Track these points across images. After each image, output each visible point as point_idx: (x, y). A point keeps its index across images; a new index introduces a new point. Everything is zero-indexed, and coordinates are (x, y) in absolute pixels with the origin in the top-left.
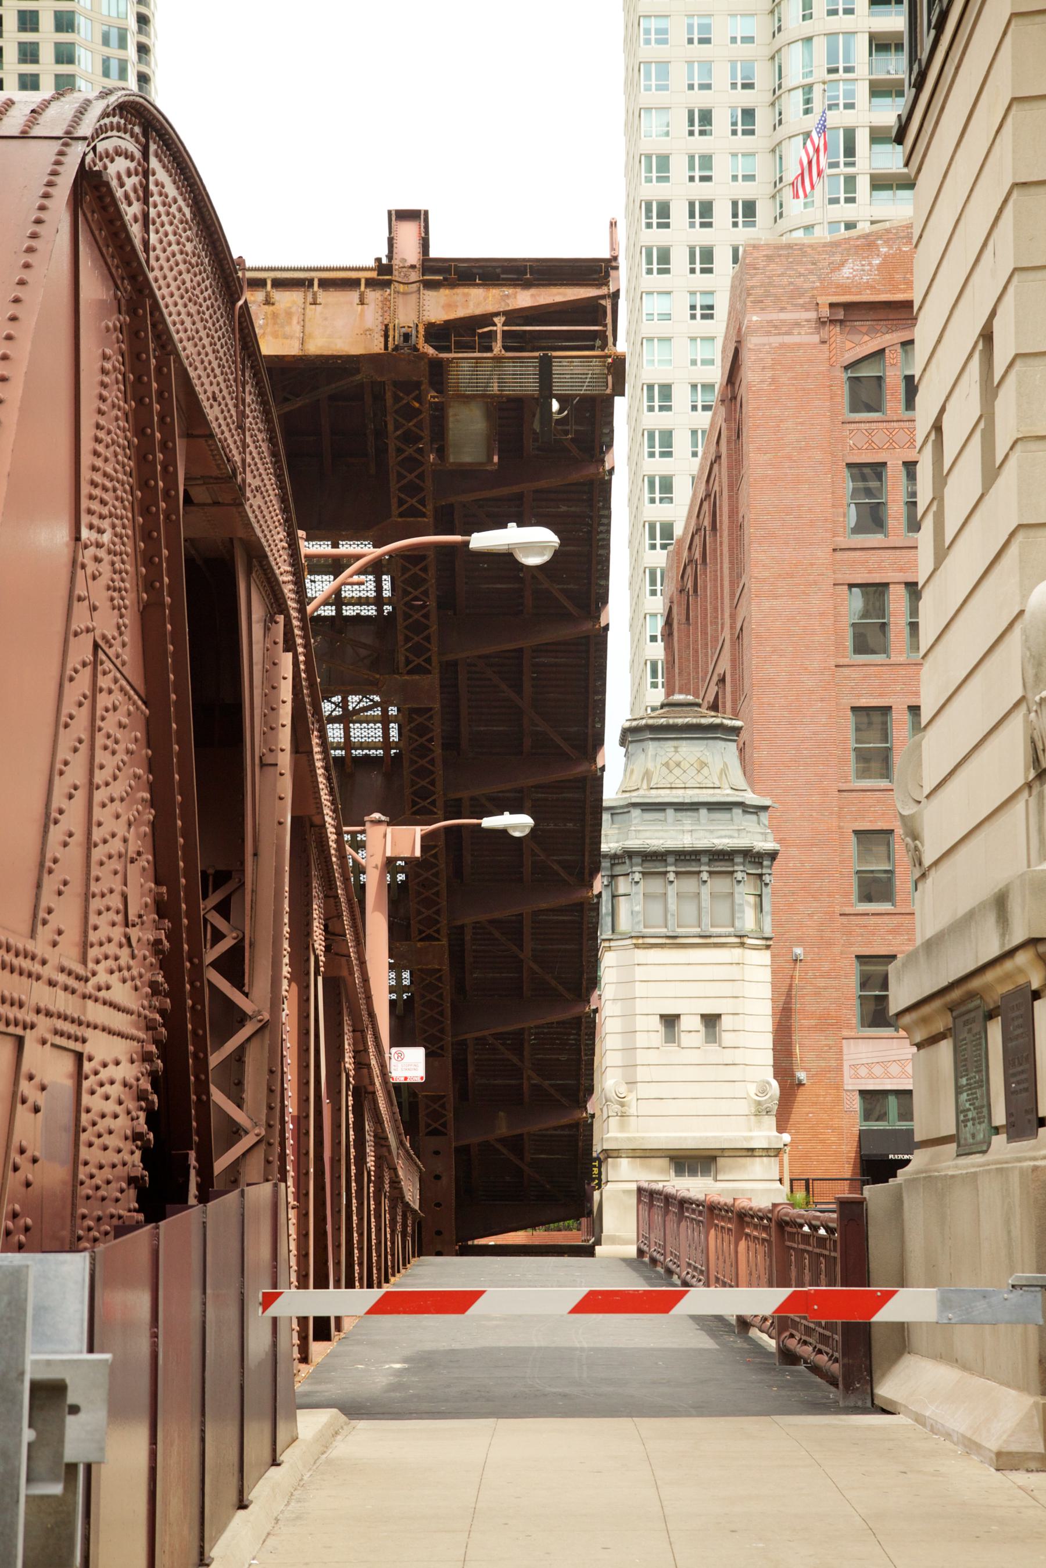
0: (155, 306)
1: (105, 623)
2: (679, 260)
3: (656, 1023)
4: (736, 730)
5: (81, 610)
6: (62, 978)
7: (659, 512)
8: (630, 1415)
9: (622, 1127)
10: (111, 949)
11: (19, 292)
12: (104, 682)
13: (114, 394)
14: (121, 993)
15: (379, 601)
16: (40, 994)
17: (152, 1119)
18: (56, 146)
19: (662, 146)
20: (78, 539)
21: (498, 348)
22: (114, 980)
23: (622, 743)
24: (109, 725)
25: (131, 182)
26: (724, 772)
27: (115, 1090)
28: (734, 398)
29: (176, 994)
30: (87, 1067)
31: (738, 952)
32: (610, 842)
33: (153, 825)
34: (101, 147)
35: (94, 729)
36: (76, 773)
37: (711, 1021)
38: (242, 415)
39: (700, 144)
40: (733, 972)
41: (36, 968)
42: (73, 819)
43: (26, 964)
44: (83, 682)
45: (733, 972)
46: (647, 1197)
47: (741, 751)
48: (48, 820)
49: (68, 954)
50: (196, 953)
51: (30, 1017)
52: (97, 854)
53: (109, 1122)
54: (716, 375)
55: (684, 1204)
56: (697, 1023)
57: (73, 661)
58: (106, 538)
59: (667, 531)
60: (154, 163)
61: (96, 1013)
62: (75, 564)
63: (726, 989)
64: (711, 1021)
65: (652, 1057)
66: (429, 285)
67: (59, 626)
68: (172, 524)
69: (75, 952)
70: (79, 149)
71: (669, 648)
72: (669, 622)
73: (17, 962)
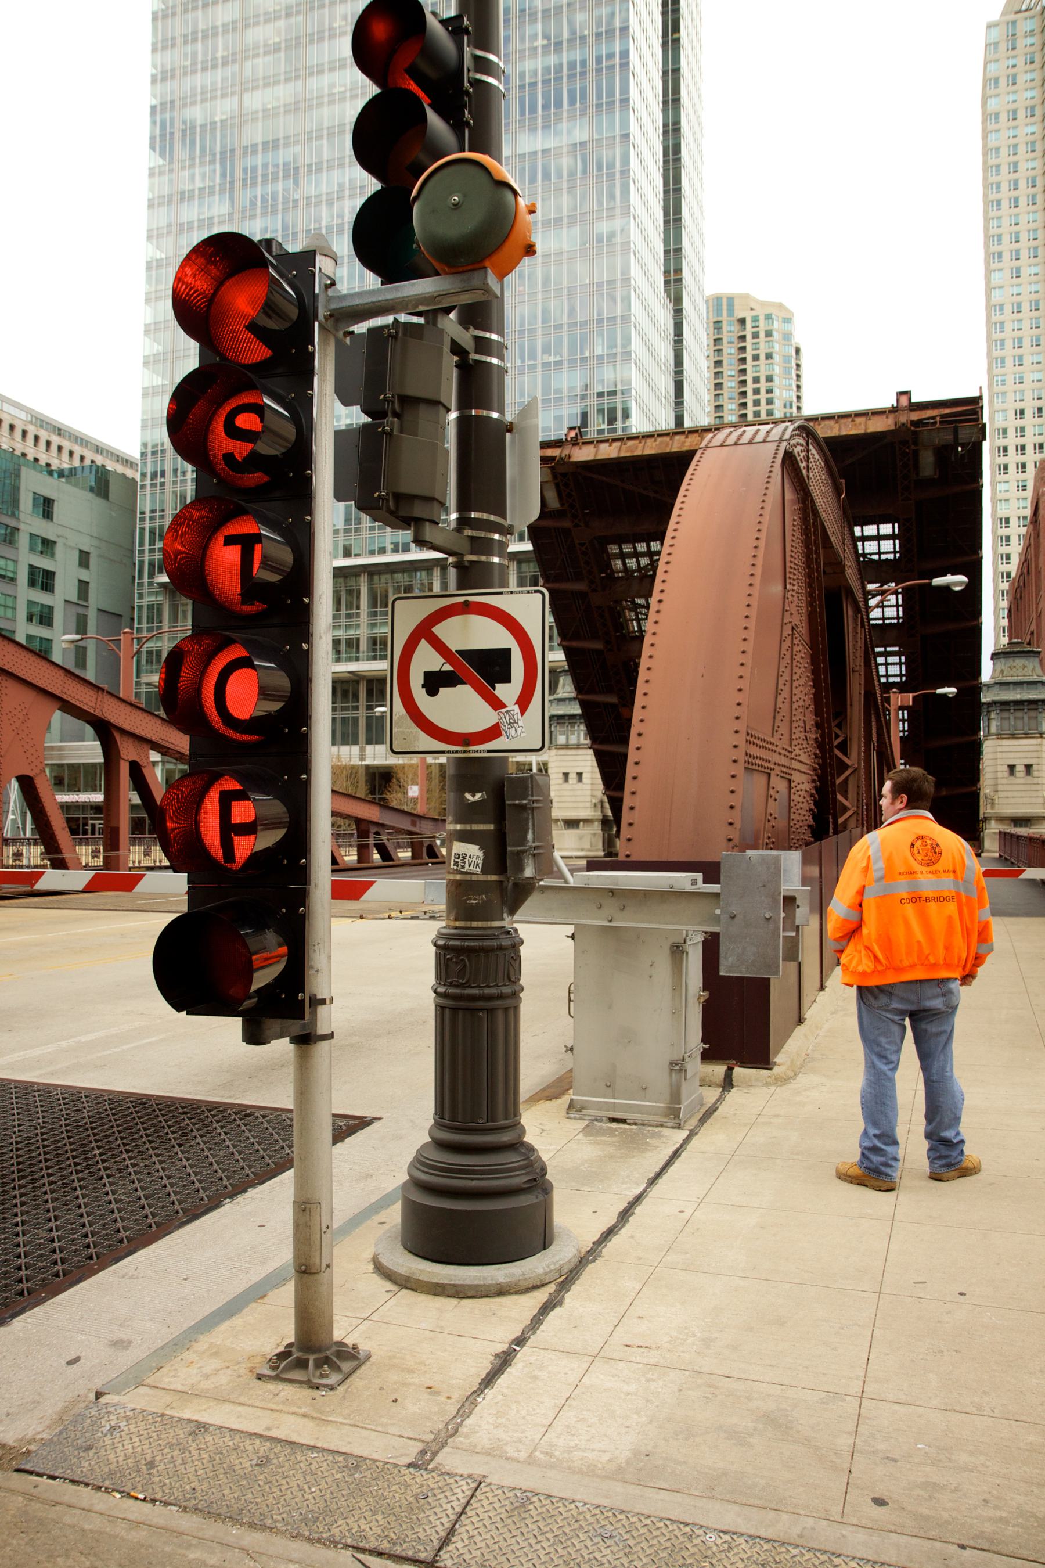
0: (812, 499)
1: (796, 620)
2: (1012, 468)
3: (1006, 768)
4: (1039, 653)
5: (787, 614)
6: (783, 752)
7: (1005, 568)
8: (1000, 916)
9: (992, 808)
10: (800, 741)
11: (764, 498)
12: (795, 642)
13: (797, 534)
14: (804, 758)
15: (898, 618)
16: (775, 758)
17: (816, 803)
18: (776, 444)
19: (1004, 425)
20: (785, 588)
21: (938, 425)
22: (801, 752)
23: (992, 659)
24: (798, 658)
25: (802, 454)
26: (1034, 669)
27: (802, 793)
28: (1036, 521)
29: (824, 758)
30: (793, 785)
31: (1039, 740)
32: (985, 698)
33: (814, 694)
34: (792, 443)
35: (792, 659)
36: (786, 677)
37: (1028, 768)
38: (844, 539)
39: (1020, 423)
40: (1038, 748)
41: (774, 748)
42: (786, 693)
43: (770, 747)
44: (788, 643)
45: (1038, 748)
46: (1003, 835)
47: (1041, 661)
48: (777, 694)
49: (785, 743)
50: (831, 742)
51: (772, 766)
52: (795, 706)
53: (800, 805)
54: (1028, 512)
55: (1018, 837)
56: (1022, 768)
57: (785, 634)
58: (795, 588)
59: (1009, 575)
60: (811, 447)
61: (796, 765)
62: (785, 598)
63: (1035, 755)
64: (1028, 768)
65: (1004, 781)
66: (911, 410)
67: (779, 622)
68: (819, 582)
69: (788, 742)
70: (785, 444)
71: (1010, 621)
72: (1010, 611)
73: (768, 746)
